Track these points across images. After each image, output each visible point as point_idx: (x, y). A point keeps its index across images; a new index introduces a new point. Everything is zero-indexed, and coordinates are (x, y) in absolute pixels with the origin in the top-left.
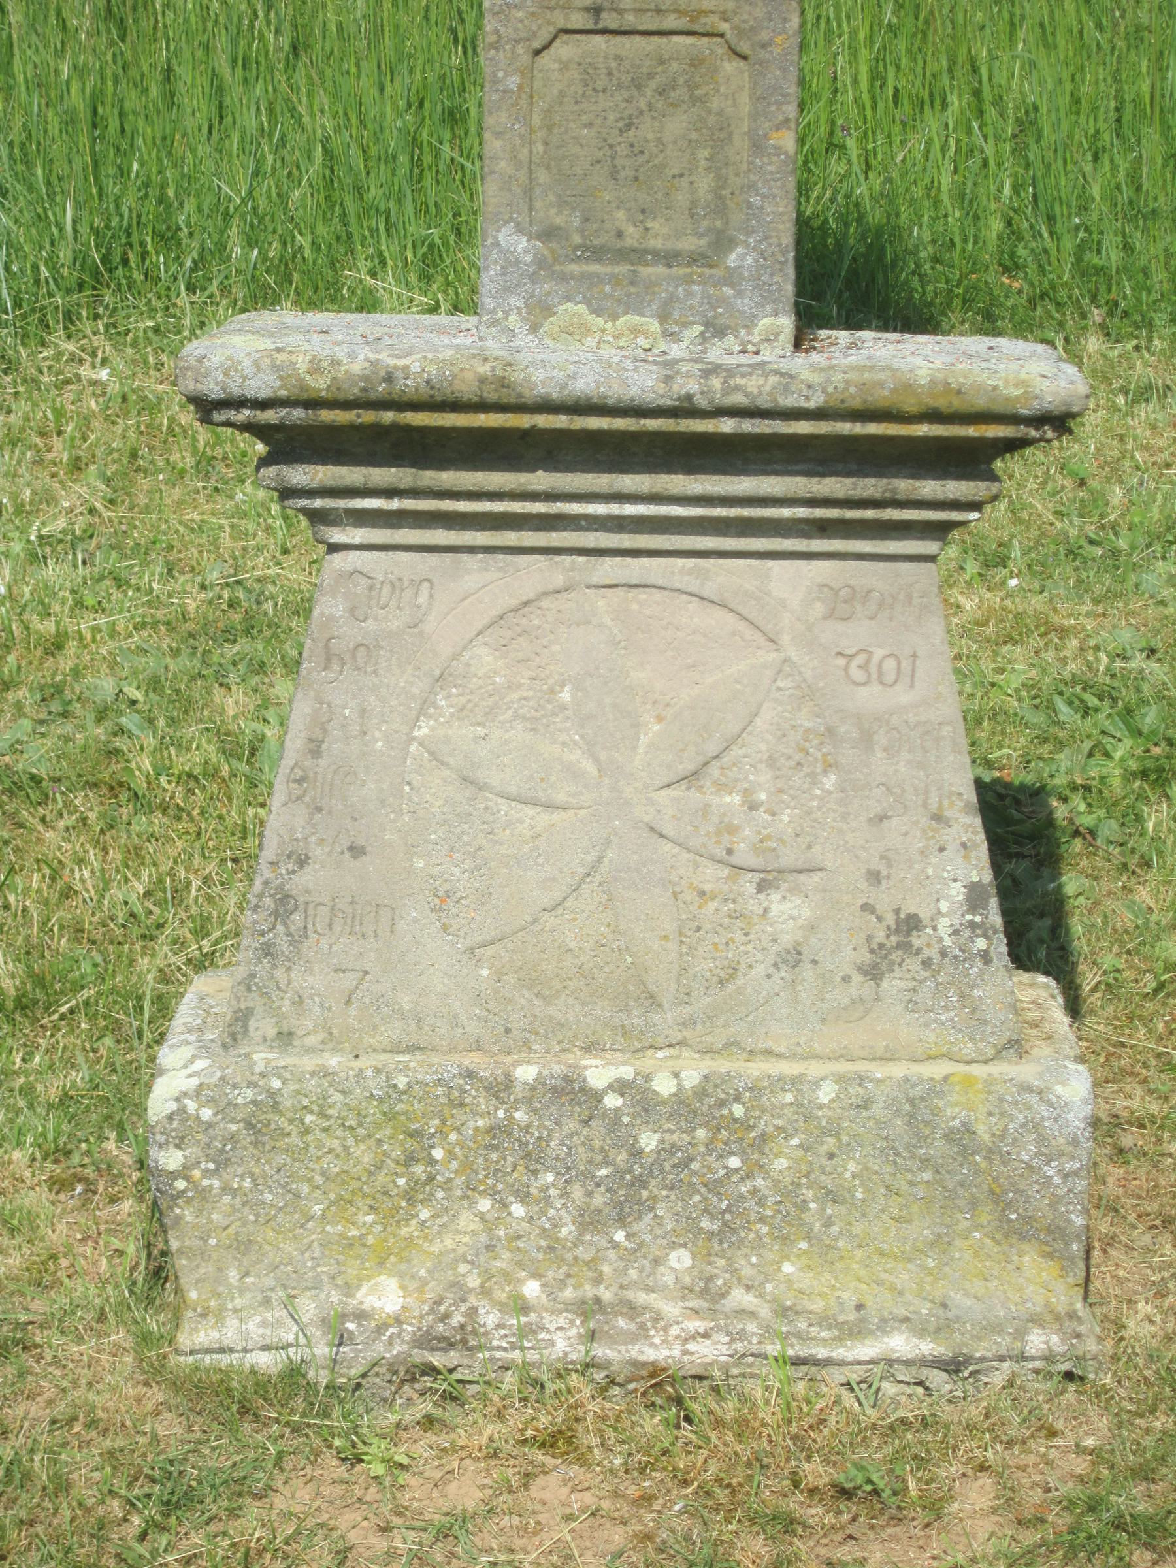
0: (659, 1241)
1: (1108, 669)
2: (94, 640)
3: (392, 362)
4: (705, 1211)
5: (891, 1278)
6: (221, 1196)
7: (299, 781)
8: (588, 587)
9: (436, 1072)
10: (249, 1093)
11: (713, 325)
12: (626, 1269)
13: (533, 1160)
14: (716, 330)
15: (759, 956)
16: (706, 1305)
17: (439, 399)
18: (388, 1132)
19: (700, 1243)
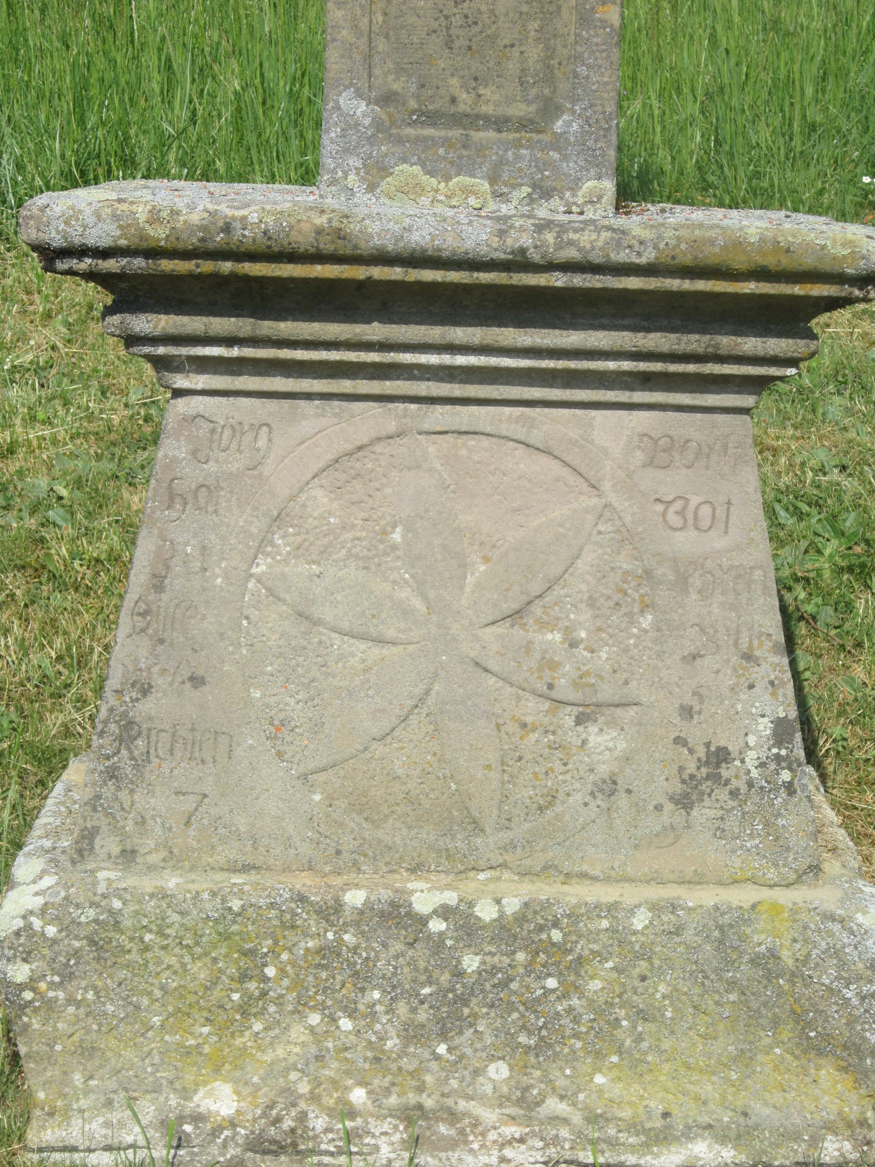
0: (478, 1054)
1: (813, 481)
2: (40, 447)
3: (229, 212)
4: (523, 1027)
5: (696, 1089)
6: (66, 1006)
7: (143, 615)
8: (420, 433)
9: (269, 896)
10: (91, 913)
11: (541, 188)
12: (447, 1078)
13: (361, 978)
14: (543, 191)
15: (577, 785)
16: (522, 1112)
17: (276, 249)
18: (223, 951)
19: (518, 1056)
